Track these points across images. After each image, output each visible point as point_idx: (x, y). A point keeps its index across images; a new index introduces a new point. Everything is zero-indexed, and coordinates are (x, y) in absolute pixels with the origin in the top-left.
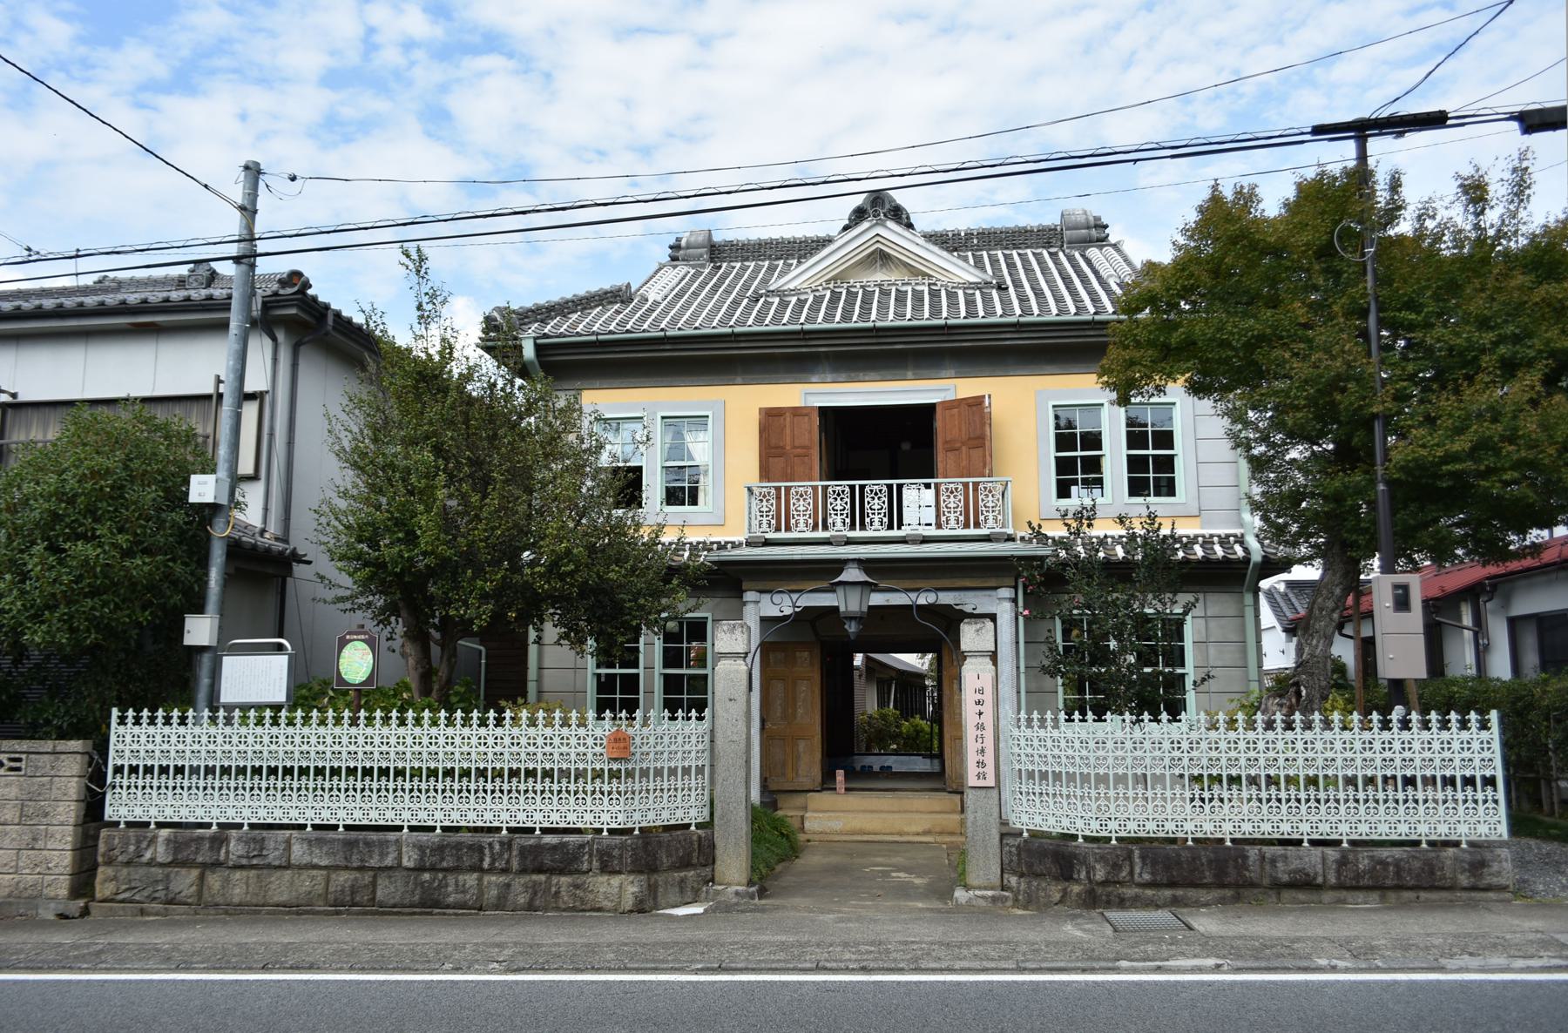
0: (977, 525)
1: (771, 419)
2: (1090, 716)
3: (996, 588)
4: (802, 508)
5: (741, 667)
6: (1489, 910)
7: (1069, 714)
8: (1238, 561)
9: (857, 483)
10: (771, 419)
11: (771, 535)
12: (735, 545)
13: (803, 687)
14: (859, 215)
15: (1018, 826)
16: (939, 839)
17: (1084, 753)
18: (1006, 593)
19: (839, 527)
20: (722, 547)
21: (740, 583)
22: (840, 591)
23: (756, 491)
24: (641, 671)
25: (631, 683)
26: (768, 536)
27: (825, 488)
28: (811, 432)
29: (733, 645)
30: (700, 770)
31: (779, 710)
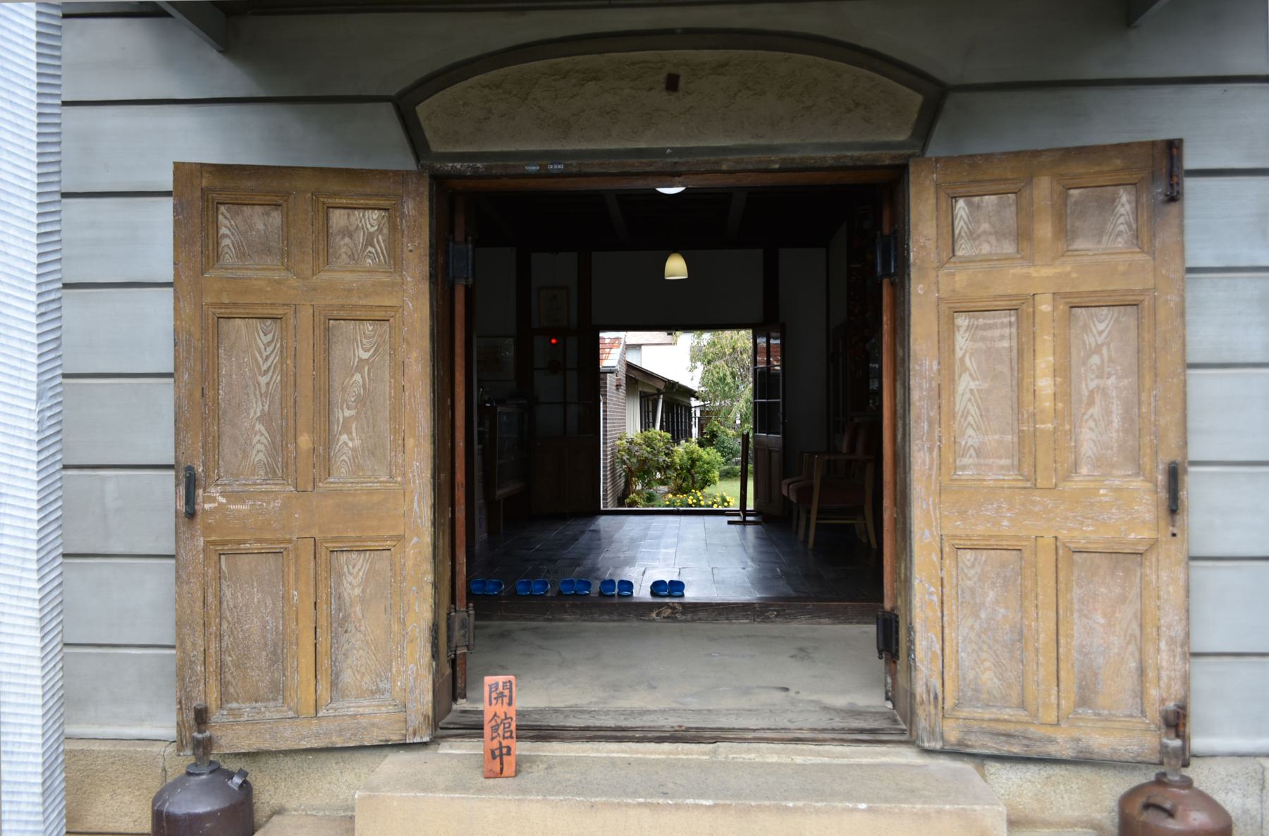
13: (359, 347)
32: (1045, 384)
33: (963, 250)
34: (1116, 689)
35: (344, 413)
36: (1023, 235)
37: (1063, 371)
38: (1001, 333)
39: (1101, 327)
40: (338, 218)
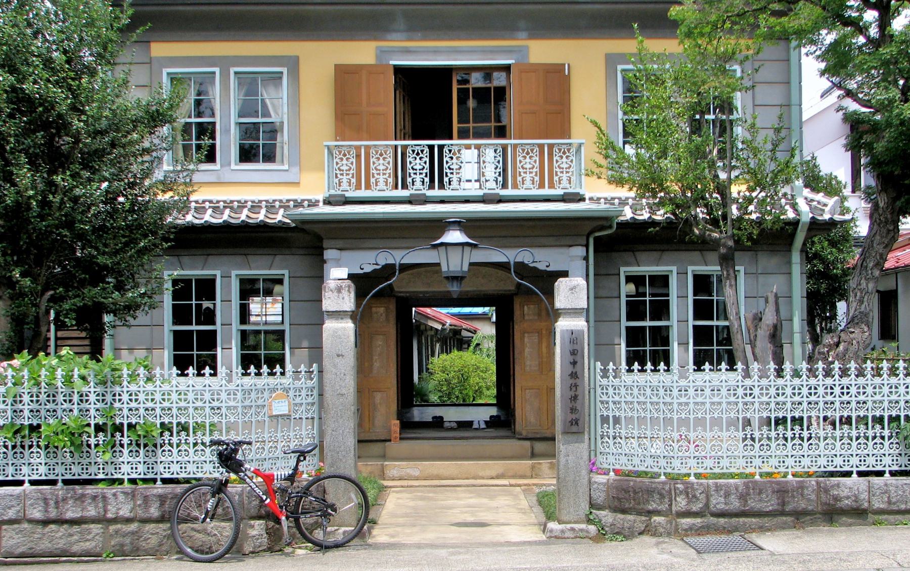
0: (552, 186)
1: (345, 75)
2: (265, 369)
4: (383, 167)
6: (803, 528)
7: (630, 363)
8: (788, 223)
9: (436, 143)
10: (345, 75)
11: (352, 194)
12: (313, 204)
13: (379, 342)
18: (580, 251)
19: (418, 187)
20: (298, 204)
21: (320, 239)
22: (442, 249)
24: (218, 327)
25: (661, 337)
26: (347, 194)
28: (385, 100)
32: (544, 350)
33: (526, 318)
35: (375, 358)
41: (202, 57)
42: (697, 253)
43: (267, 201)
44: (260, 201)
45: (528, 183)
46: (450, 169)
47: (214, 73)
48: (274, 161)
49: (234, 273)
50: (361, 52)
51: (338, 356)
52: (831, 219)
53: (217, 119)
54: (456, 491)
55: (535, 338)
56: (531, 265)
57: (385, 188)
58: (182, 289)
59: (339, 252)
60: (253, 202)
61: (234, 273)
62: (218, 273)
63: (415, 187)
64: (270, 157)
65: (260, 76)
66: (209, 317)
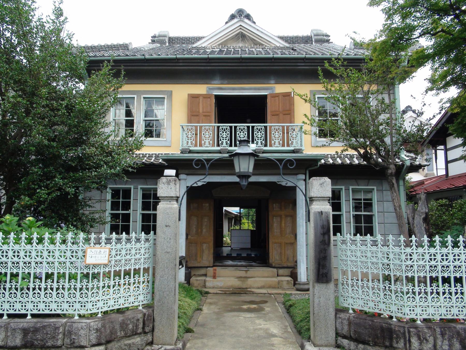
0: (288, 145)
1: (193, 98)
3: (297, 174)
5: (175, 205)
10: (193, 98)
14: (233, 17)
15: (346, 306)
16: (270, 291)
17: (397, 262)
23: (185, 128)
25: (126, 218)
27: (218, 127)
29: (171, 187)
30: (146, 270)
31: (195, 230)
33: (275, 209)
34: (291, 259)
35: (204, 227)
36: (281, 208)
37: (285, 223)
38: (279, 219)
39: (289, 219)
40: (204, 204)
41: (129, 91)
42: (354, 180)
43: (155, 154)
44: (153, 154)
45: (277, 144)
46: (257, 137)
47: (134, 98)
48: (159, 137)
49: (139, 187)
50: (200, 89)
51: (166, 226)
52: (419, 164)
53: (154, 139)
54: (241, 296)
55: (279, 219)
56: (278, 183)
57: (209, 146)
58: (115, 193)
59: (186, 176)
60: (149, 154)
61: (139, 187)
62: (132, 187)
63: (223, 146)
64: (158, 136)
65: (155, 99)
66: (127, 206)
